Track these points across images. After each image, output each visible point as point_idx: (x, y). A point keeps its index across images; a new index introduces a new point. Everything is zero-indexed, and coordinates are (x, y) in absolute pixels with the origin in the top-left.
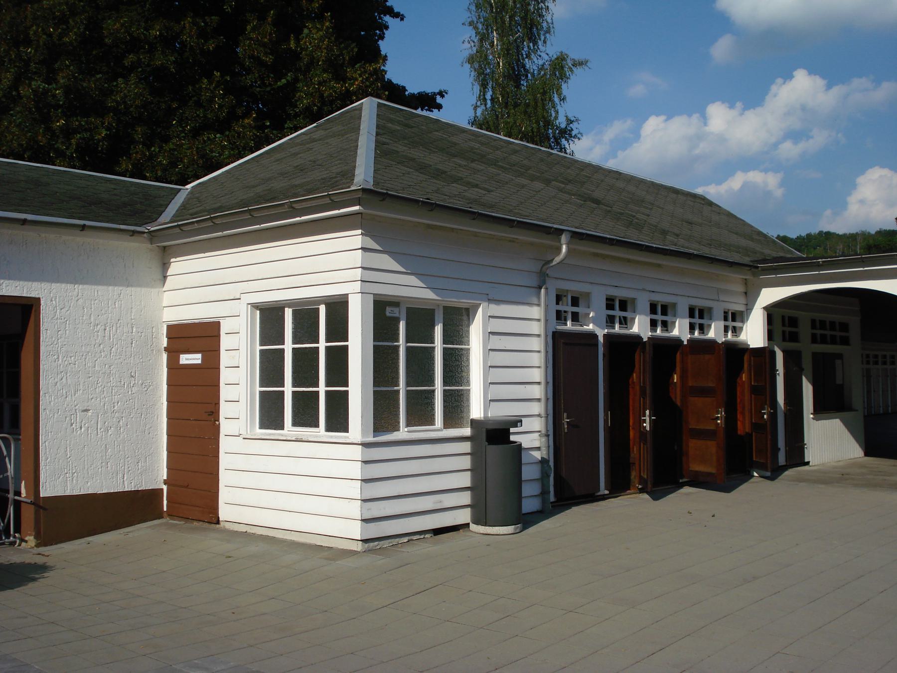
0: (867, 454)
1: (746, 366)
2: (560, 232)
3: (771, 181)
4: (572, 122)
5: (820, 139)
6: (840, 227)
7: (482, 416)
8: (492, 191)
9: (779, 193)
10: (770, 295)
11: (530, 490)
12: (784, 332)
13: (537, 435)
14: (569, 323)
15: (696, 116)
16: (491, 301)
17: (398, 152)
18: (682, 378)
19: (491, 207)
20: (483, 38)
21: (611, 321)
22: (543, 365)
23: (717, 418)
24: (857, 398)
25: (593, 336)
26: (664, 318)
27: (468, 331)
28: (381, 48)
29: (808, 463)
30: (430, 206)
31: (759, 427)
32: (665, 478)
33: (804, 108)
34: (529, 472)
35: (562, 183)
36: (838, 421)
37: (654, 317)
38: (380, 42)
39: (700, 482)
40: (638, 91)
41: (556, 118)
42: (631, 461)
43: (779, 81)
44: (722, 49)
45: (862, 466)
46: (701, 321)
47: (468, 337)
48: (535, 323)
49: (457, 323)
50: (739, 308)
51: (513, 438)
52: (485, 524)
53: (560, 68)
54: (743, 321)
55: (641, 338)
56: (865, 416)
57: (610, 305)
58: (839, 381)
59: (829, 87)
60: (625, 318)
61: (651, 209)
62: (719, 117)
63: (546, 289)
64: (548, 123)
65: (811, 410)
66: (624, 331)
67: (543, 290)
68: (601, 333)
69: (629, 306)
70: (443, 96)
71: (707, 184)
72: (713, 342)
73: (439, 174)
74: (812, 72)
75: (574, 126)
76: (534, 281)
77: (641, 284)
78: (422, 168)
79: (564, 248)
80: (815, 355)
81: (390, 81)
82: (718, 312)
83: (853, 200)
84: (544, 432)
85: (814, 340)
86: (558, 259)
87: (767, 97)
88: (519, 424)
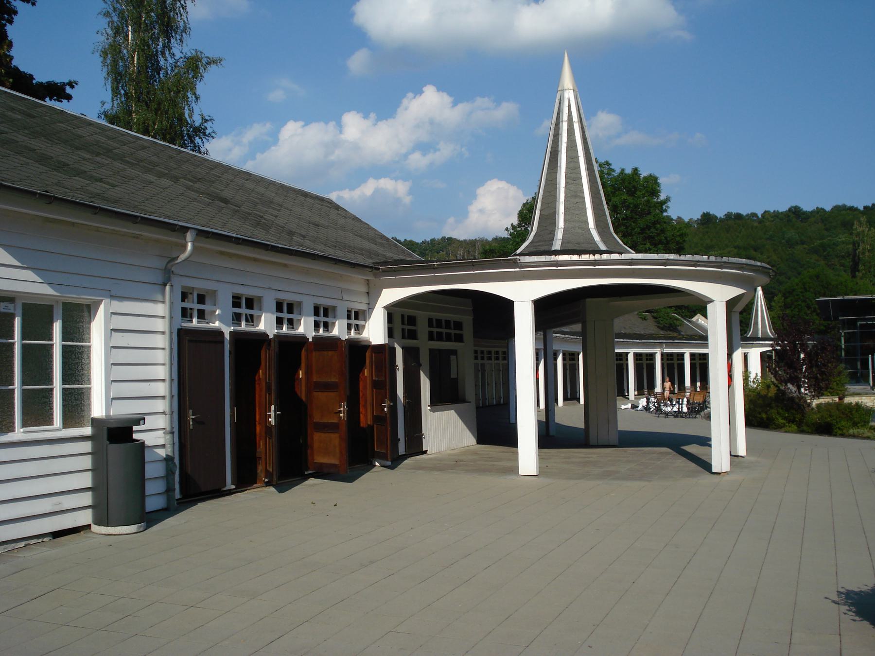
0: (480, 441)
1: (368, 361)
2: (185, 230)
3: (398, 188)
4: (206, 121)
5: (445, 151)
6: (461, 233)
7: (104, 414)
8: (116, 186)
9: (407, 200)
10: (391, 295)
11: (154, 489)
12: (403, 330)
13: (162, 432)
14: (195, 320)
15: (332, 124)
16: (113, 297)
17: (17, 142)
18: (308, 374)
19: (116, 202)
20: (118, 31)
21: (237, 318)
22: (167, 362)
23: (340, 412)
24: (469, 390)
25: (219, 333)
26: (290, 316)
27: (89, 328)
28: (9, 34)
29: (426, 452)
30: (50, 199)
31: (379, 419)
32: (291, 470)
33: (432, 122)
34: (153, 470)
35: (190, 180)
36: (453, 412)
37: (280, 315)
38: (8, 27)
39: (324, 473)
40: (277, 96)
41: (191, 116)
42: (258, 455)
43: (410, 95)
44: (358, 62)
45: (475, 453)
46: (326, 319)
47: (89, 334)
48: (160, 320)
49: (77, 320)
50: (362, 307)
51: (135, 436)
52: (108, 524)
53: (194, 65)
54: (365, 320)
55: (267, 336)
56: (478, 408)
57: (236, 303)
58: (453, 375)
59: (455, 104)
60: (251, 316)
61: (279, 210)
62: (354, 126)
63: (172, 286)
64: (181, 119)
65: (429, 402)
66: (251, 329)
67: (168, 288)
68: (227, 330)
69: (255, 305)
70: (72, 87)
71: (342, 189)
72: (336, 340)
73: (61, 166)
74: (440, 89)
75: (208, 125)
76: (159, 278)
77: (268, 282)
78: (43, 159)
79: (189, 246)
80: (431, 351)
81: (16, 69)
82: (342, 310)
83: (474, 208)
84: (168, 429)
85: (431, 337)
86: (183, 257)
87: (399, 110)
88: (142, 422)
